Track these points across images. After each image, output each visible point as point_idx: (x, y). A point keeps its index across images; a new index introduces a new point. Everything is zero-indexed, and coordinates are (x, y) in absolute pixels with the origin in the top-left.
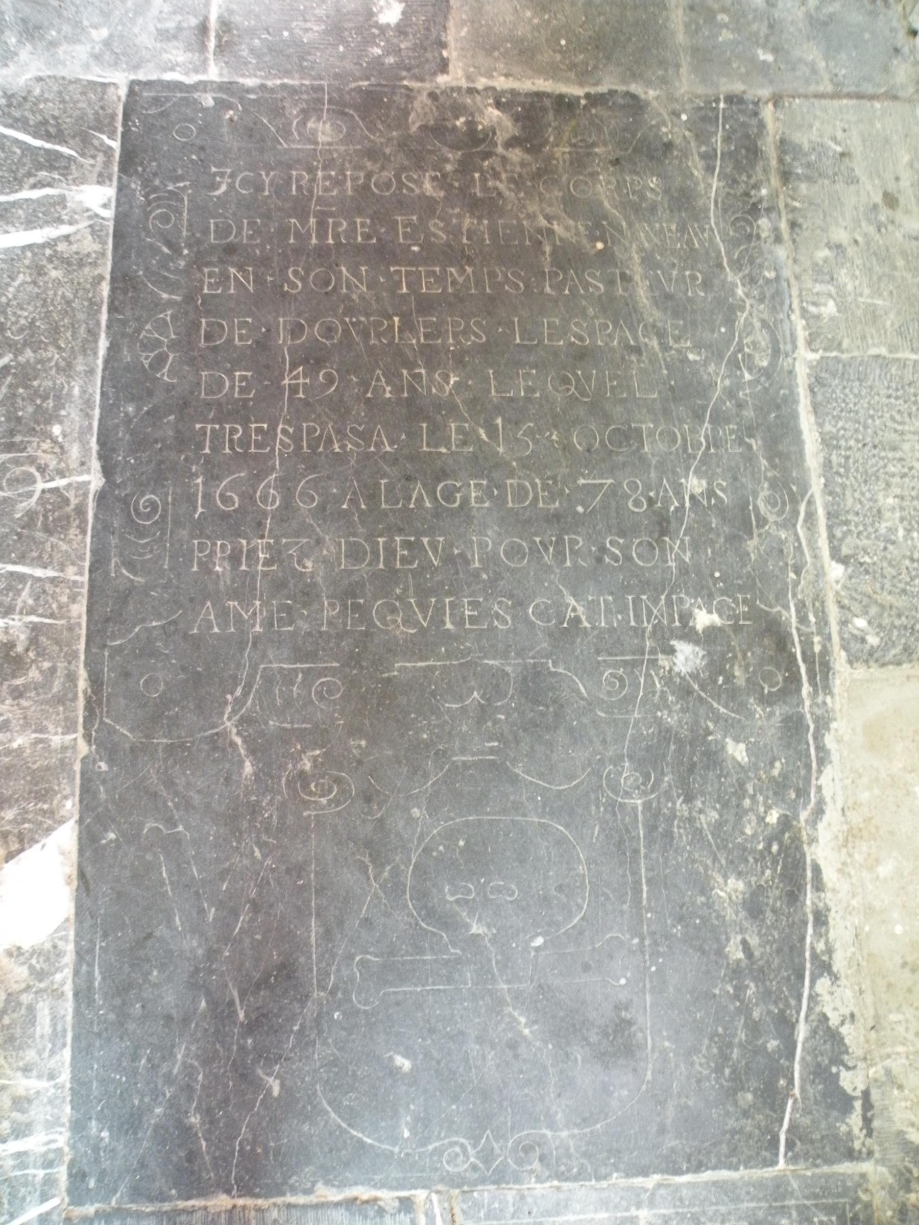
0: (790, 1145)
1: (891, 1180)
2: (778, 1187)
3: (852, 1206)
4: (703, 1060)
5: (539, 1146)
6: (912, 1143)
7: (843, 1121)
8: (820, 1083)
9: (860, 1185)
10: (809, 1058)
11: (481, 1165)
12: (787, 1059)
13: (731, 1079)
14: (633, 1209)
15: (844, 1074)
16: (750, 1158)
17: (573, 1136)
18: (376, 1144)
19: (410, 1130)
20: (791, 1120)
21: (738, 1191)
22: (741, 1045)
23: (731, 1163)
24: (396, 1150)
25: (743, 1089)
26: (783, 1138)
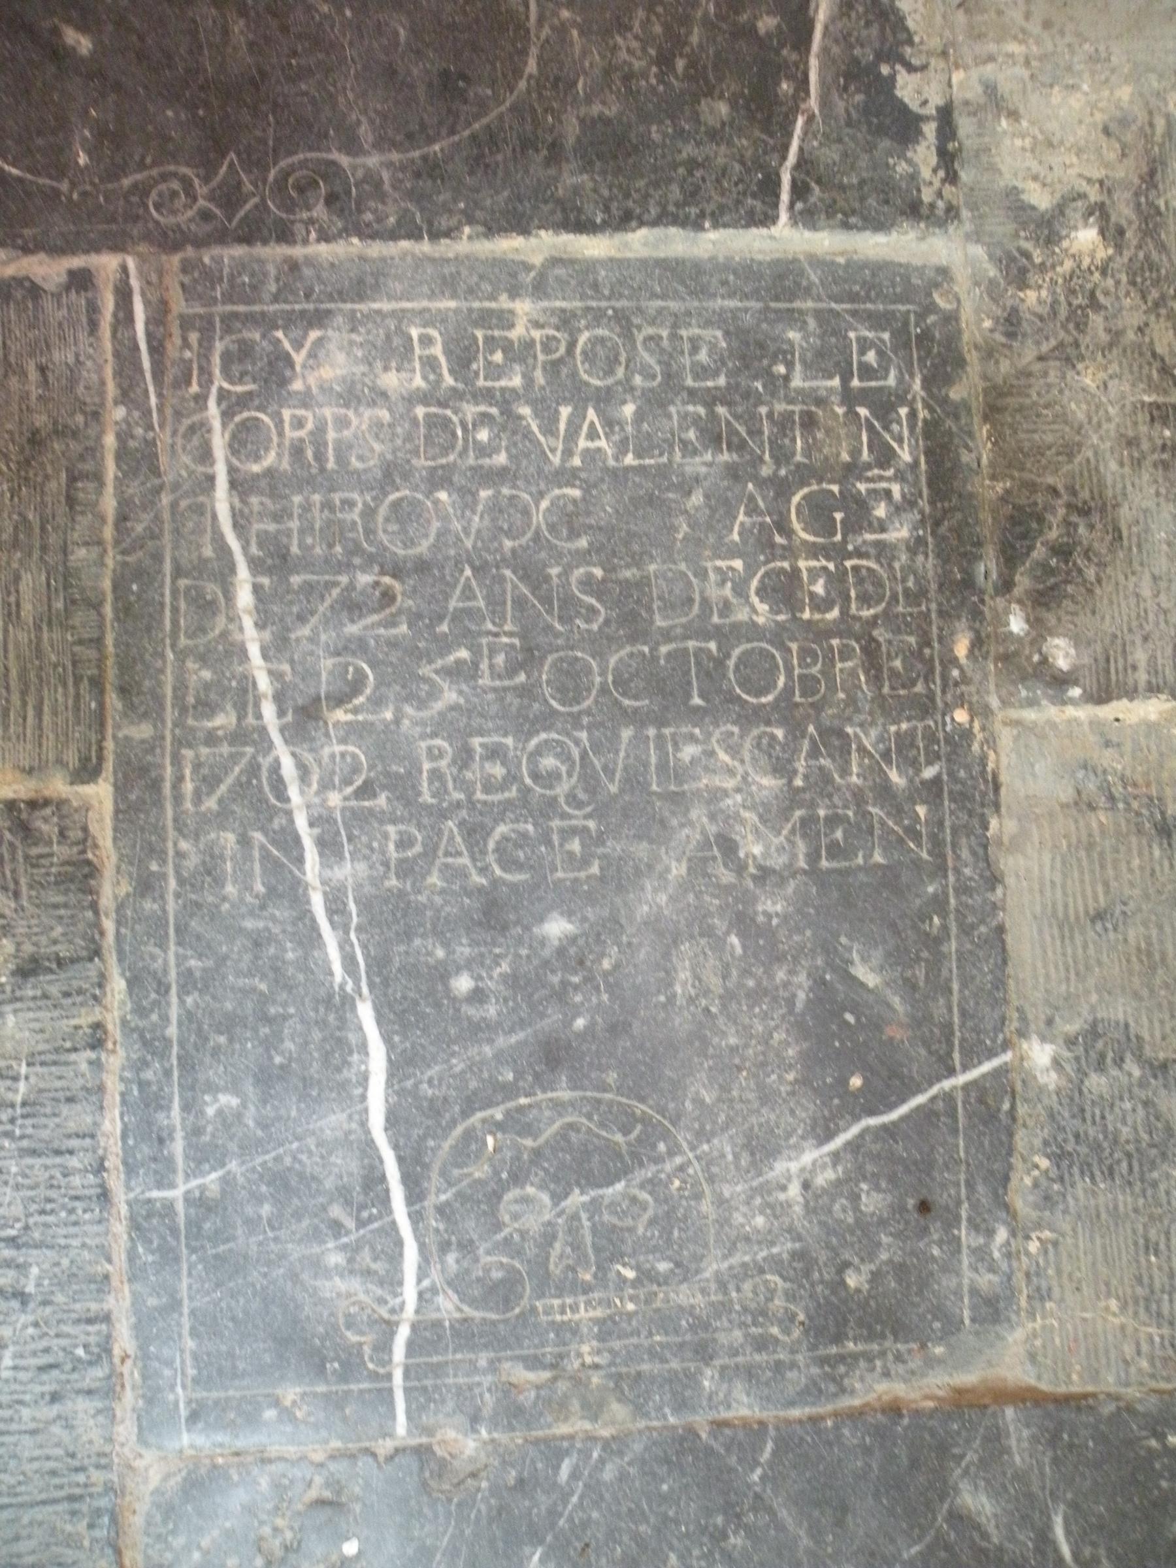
0: (800, 191)
1: (992, 272)
2: (781, 277)
3: (921, 317)
4: (635, 44)
5: (325, 178)
6: (1033, 208)
7: (902, 156)
8: (858, 91)
9: (937, 285)
10: (836, 50)
11: (218, 212)
12: (795, 47)
13: (687, 77)
14: (504, 297)
15: (902, 77)
16: (722, 209)
17: (390, 165)
18: (29, 176)
19: (89, 153)
20: (801, 149)
21: (705, 279)
22: (706, 22)
23: (687, 217)
24: (64, 186)
25: (709, 93)
26: (786, 179)
